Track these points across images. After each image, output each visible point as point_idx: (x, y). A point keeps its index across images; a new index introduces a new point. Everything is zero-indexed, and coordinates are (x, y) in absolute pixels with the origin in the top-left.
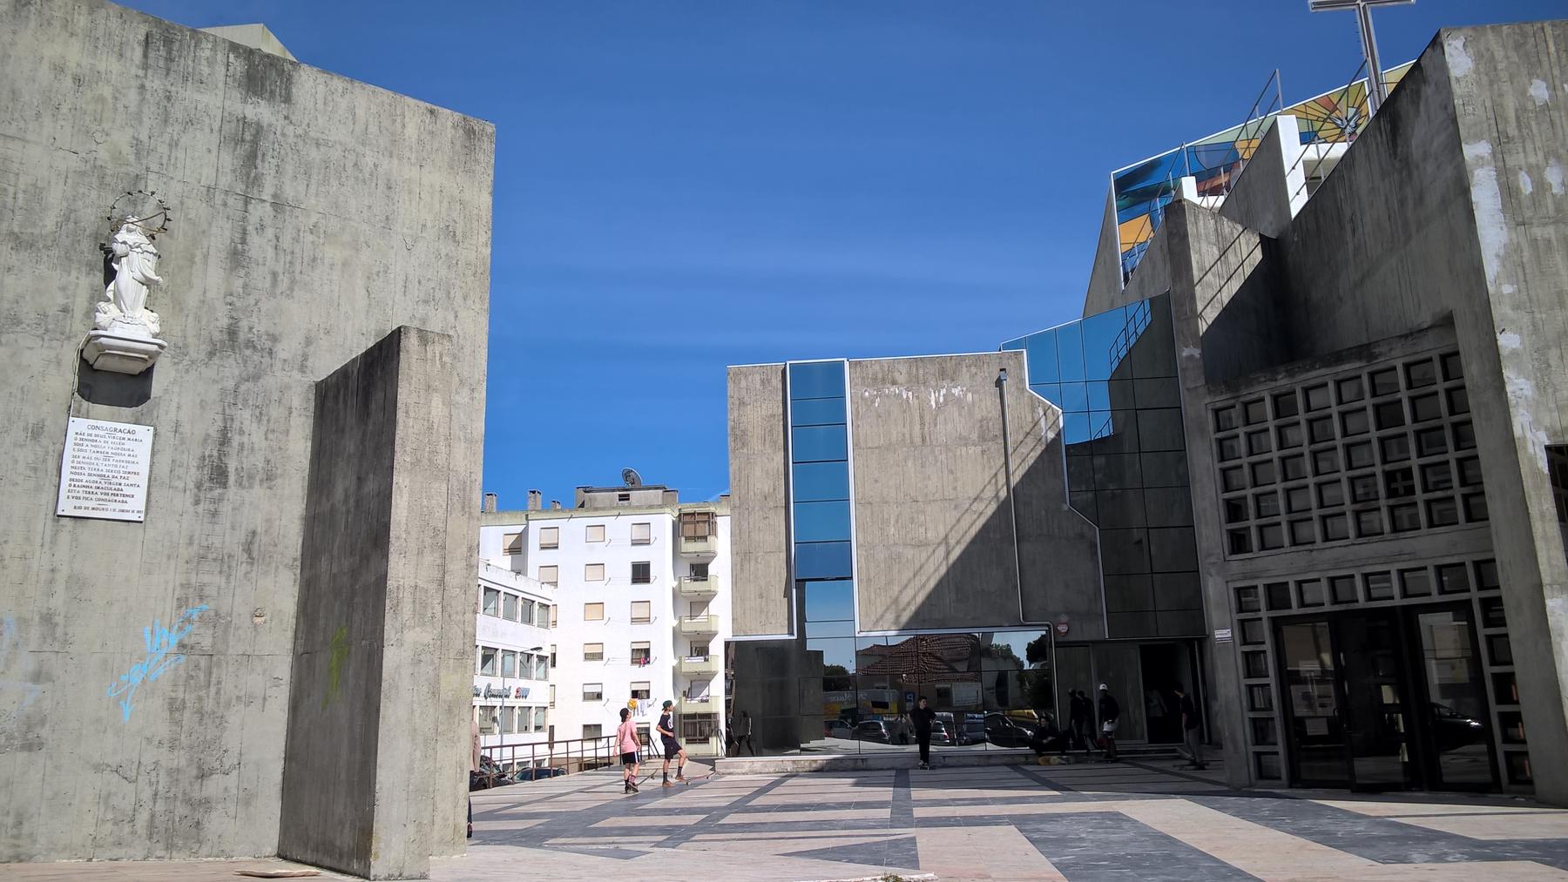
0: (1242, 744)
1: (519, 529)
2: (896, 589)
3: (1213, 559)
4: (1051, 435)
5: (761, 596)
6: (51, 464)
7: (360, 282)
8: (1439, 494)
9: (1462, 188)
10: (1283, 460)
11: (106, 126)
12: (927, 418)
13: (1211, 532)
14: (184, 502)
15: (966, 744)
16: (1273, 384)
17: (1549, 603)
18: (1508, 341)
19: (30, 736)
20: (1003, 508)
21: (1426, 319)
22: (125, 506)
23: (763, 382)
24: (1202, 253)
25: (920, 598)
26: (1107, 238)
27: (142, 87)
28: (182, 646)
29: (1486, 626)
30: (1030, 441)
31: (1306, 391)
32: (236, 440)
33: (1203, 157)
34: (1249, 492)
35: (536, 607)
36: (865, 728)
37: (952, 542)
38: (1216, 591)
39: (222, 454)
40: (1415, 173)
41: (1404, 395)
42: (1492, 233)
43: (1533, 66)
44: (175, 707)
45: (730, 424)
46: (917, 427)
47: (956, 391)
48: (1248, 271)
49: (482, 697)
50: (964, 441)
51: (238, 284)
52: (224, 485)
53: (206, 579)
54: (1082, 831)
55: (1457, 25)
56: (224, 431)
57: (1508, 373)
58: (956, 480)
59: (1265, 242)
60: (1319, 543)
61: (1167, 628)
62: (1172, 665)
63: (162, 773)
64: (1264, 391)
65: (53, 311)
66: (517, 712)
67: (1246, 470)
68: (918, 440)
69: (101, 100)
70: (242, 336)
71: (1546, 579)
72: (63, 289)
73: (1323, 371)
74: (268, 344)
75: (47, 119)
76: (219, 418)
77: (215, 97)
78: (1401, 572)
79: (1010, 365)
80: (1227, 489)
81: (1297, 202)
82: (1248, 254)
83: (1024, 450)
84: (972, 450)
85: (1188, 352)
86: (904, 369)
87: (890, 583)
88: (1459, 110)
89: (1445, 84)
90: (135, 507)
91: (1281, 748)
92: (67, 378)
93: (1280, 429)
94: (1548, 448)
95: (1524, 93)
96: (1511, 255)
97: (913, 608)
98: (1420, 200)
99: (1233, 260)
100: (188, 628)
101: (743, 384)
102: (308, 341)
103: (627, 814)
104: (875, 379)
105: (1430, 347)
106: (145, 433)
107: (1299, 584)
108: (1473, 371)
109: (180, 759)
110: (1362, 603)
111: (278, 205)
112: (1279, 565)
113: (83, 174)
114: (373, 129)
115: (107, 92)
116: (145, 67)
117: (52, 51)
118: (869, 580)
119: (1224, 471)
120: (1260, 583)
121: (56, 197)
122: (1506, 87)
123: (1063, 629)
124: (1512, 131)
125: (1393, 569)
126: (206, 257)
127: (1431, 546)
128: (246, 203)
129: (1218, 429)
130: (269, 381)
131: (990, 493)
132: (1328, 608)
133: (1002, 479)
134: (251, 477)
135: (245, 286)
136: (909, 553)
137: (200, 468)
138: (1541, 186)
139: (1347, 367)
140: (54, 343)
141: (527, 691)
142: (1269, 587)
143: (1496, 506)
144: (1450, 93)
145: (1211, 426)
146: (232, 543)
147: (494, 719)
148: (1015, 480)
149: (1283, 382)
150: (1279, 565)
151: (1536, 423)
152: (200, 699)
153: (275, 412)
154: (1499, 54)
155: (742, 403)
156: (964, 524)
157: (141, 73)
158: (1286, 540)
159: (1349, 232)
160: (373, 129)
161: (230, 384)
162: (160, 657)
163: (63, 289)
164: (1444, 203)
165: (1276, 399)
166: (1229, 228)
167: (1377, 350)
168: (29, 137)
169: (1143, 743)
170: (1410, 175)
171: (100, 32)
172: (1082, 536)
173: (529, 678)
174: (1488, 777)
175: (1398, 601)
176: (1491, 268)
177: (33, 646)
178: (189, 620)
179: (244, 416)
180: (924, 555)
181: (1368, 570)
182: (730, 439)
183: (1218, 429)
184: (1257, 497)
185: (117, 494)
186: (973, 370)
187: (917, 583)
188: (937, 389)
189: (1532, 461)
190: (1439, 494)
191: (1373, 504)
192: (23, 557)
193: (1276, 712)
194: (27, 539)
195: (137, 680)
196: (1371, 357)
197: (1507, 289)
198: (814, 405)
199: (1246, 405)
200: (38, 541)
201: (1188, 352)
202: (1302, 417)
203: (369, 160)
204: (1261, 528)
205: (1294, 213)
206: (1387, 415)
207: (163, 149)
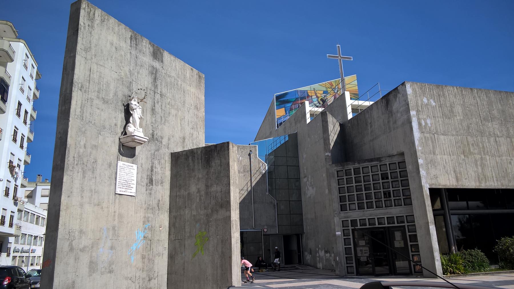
0: (343, 264)
1: (32, 189)
3: (336, 212)
4: (264, 172)
6: (114, 177)
7: (179, 121)
8: (398, 198)
11: (123, 64)
14: (144, 189)
16: (354, 166)
17: (430, 227)
18: (420, 161)
19: (111, 268)
20: (249, 193)
21: (395, 152)
22: (131, 191)
26: (270, 113)
27: (131, 53)
28: (144, 237)
29: (409, 232)
30: (258, 173)
32: (154, 170)
33: (299, 93)
35: (41, 218)
39: (152, 175)
40: (394, 115)
41: (389, 172)
42: (417, 134)
43: (424, 93)
44: (143, 257)
49: (20, 253)
51: (154, 119)
52: (152, 184)
53: (149, 215)
55: (413, 80)
56: (152, 167)
57: (421, 169)
63: (141, 280)
65: (113, 125)
66: (31, 258)
69: (121, 56)
70: (155, 137)
71: (429, 221)
72: (115, 118)
73: (368, 163)
74: (161, 140)
75: (109, 61)
76: (151, 163)
77: (147, 59)
79: (253, 150)
81: (350, 116)
83: (256, 176)
88: (409, 102)
89: (405, 95)
90: (132, 191)
92: (115, 149)
94: (429, 189)
95: (422, 100)
96: (420, 139)
98: (395, 122)
100: (146, 231)
102: (169, 139)
103: (319, 285)
105: (396, 160)
106: (135, 167)
108: (409, 168)
109: (144, 275)
110: (377, 225)
111: (161, 95)
112: (356, 215)
113: (118, 80)
114: (180, 73)
115: (123, 53)
116: (131, 46)
117: (110, 38)
120: (349, 219)
121: (112, 86)
122: (419, 98)
123: (265, 230)
124: (420, 109)
126: (147, 110)
127: (395, 211)
128: (155, 94)
130: (161, 151)
131: (245, 188)
133: (249, 184)
134: (158, 182)
135: (155, 120)
137: (147, 179)
138: (426, 124)
139: (374, 163)
140: (114, 136)
141: (35, 250)
143: (415, 202)
144: (407, 98)
145: (336, 176)
146: (154, 203)
147: (23, 261)
148: (253, 184)
149: (357, 165)
151: (426, 182)
152: (149, 255)
153: (163, 161)
154: (417, 90)
157: (130, 48)
159: (369, 126)
160: (180, 73)
161: (153, 152)
162: (139, 241)
163: (115, 118)
164: (403, 124)
167: (382, 159)
168: (106, 66)
170: (392, 115)
171: (120, 33)
172: (271, 203)
173: (36, 245)
174: (409, 271)
176: (417, 143)
177: (111, 238)
178: (145, 229)
179: (156, 162)
181: (379, 217)
183: (338, 177)
185: (129, 187)
186: (242, 150)
189: (426, 191)
190: (398, 198)
191: (381, 200)
192: (108, 208)
193: (353, 255)
194: (108, 201)
195: (134, 249)
196: (380, 161)
197: (420, 148)
199: (346, 170)
200: (111, 202)
203: (180, 83)
207: (136, 74)
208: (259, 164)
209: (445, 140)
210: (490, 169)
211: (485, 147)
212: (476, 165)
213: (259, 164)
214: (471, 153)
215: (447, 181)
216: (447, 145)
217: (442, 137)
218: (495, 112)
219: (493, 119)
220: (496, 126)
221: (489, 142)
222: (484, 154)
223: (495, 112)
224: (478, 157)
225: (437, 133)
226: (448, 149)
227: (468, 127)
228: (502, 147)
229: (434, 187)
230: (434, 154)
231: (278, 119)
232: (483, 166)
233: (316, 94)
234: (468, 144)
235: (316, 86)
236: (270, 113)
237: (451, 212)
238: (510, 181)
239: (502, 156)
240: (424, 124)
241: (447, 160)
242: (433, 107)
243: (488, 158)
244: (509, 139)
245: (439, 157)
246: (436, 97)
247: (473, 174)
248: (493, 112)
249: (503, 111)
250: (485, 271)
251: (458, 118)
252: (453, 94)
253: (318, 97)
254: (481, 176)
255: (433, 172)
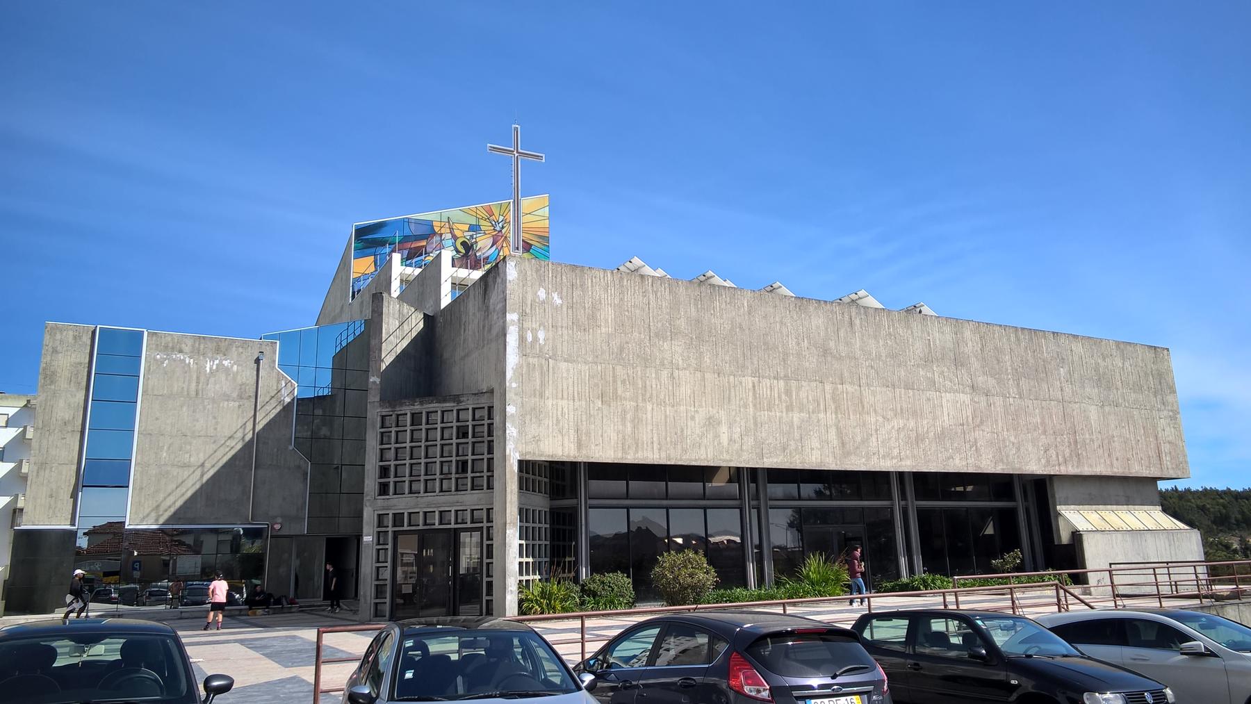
2: (162, 496)
4: (288, 400)
5: (51, 496)
9: (504, 334)
10: (412, 448)
12: (202, 379)
13: (371, 483)
15: (186, 604)
18: (511, 409)
20: (248, 446)
23: (75, 337)
24: (390, 324)
25: (179, 504)
26: (345, 265)
30: (274, 403)
31: (428, 413)
33: (413, 227)
34: (392, 463)
36: (98, 593)
37: (208, 465)
38: (369, 515)
41: (470, 424)
42: (512, 358)
43: (541, 281)
45: (43, 365)
46: (193, 385)
47: (226, 363)
48: (414, 334)
50: (227, 397)
54: (275, 643)
58: (217, 423)
59: (426, 317)
60: (422, 494)
61: (344, 530)
62: (341, 550)
64: (407, 410)
67: (393, 451)
68: (193, 393)
78: (457, 511)
79: (267, 350)
80: (381, 460)
81: (445, 301)
82: (416, 324)
83: (268, 408)
84: (231, 404)
85: (374, 379)
86: (190, 342)
87: (157, 491)
91: (388, 600)
93: (412, 431)
96: (519, 367)
97: (172, 510)
99: (406, 327)
101: (58, 337)
104: (166, 347)
105: (483, 401)
107: (410, 514)
110: (437, 526)
112: (402, 504)
118: (141, 489)
119: (382, 450)
120: (391, 512)
123: (277, 527)
124: (528, 311)
125: (453, 509)
127: (470, 499)
129: (382, 427)
131: (239, 435)
132: (421, 527)
133: (250, 426)
136: (175, 471)
138: (536, 339)
142: (394, 514)
143: (497, 485)
148: (259, 428)
149: (417, 407)
150: (402, 504)
154: (529, 273)
155: (55, 351)
156: (219, 454)
158: (407, 491)
165: (413, 415)
166: (407, 309)
169: (319, 601)
172: (299, 467)
175: (453, 526)
176: (509, 374)
180: (186, 474)
182: (41, 377)
183: (382, 427)
184: (396, 466)
187: (179, 492)
188: (213, 359)
189: (511, 466)
196: (459, 402)
197: (514, 385)
198: (115, 363)
201: (374, 379)
202: (424, 427)
204: (395, 483)
205: (442, 307)
206: (462, 433)
208: (278, 381)
209: (568, 370)
210: (650, 427)
211: (649, 388)
212: (624, 419)
213: (278, 381)
214: (616, 397)
215: (558, 446)
216: (571, 381)
217: (563, 365)
218: (682, 323)
219: (674, 334)
220: (677, 349)
221: (658, 378)
222: (644, 400)
223: (682, 323)
224: (630, 405)
225: (554, 357)
226: (571, 388)
227: (621, 349)
228: (683, 389)
229: (528, 458)
230: (541, 396)
231: (357, 280)
232: (636, 422)
233: (451, 229)
234: (615, 381)
235: (455, 213)
236: (345, 265)
237: (590, 502)
238: (685, 451)
239: (679, 404)
240: (530, 339)
241: (565, 410)
242: (557, 309)
243: (649, 408)
244: (698, 374)
245: (549, 403)
246: (565, 290)
247: (614, 436)
248: (678, 322)
249: (698, 321)
250: (564, 609)
251: (603, 330)
252: (603, 284)
253: (455, 238)
254: (629, 441)
255: (533, 430)
